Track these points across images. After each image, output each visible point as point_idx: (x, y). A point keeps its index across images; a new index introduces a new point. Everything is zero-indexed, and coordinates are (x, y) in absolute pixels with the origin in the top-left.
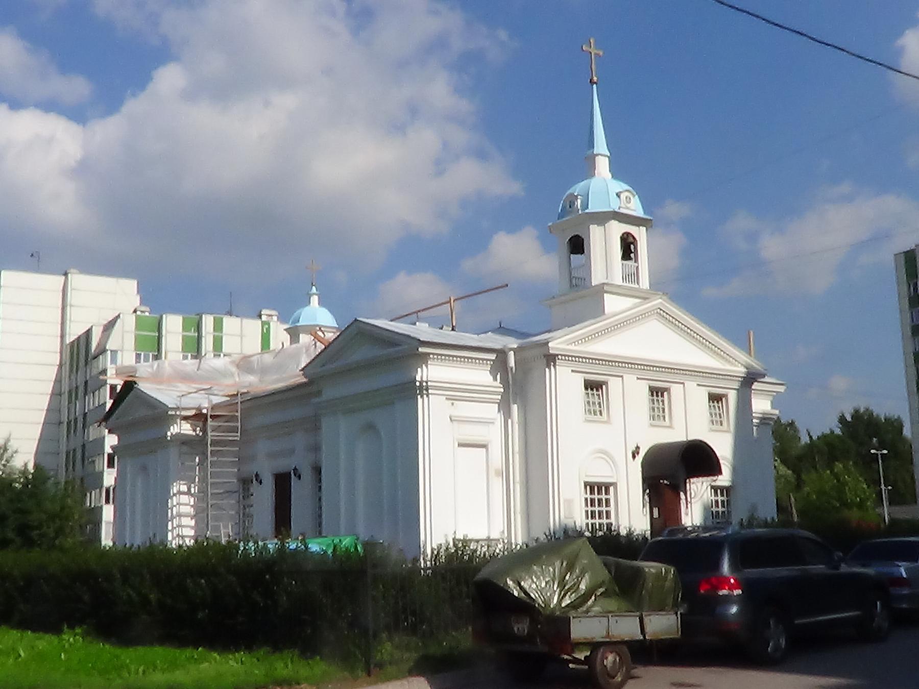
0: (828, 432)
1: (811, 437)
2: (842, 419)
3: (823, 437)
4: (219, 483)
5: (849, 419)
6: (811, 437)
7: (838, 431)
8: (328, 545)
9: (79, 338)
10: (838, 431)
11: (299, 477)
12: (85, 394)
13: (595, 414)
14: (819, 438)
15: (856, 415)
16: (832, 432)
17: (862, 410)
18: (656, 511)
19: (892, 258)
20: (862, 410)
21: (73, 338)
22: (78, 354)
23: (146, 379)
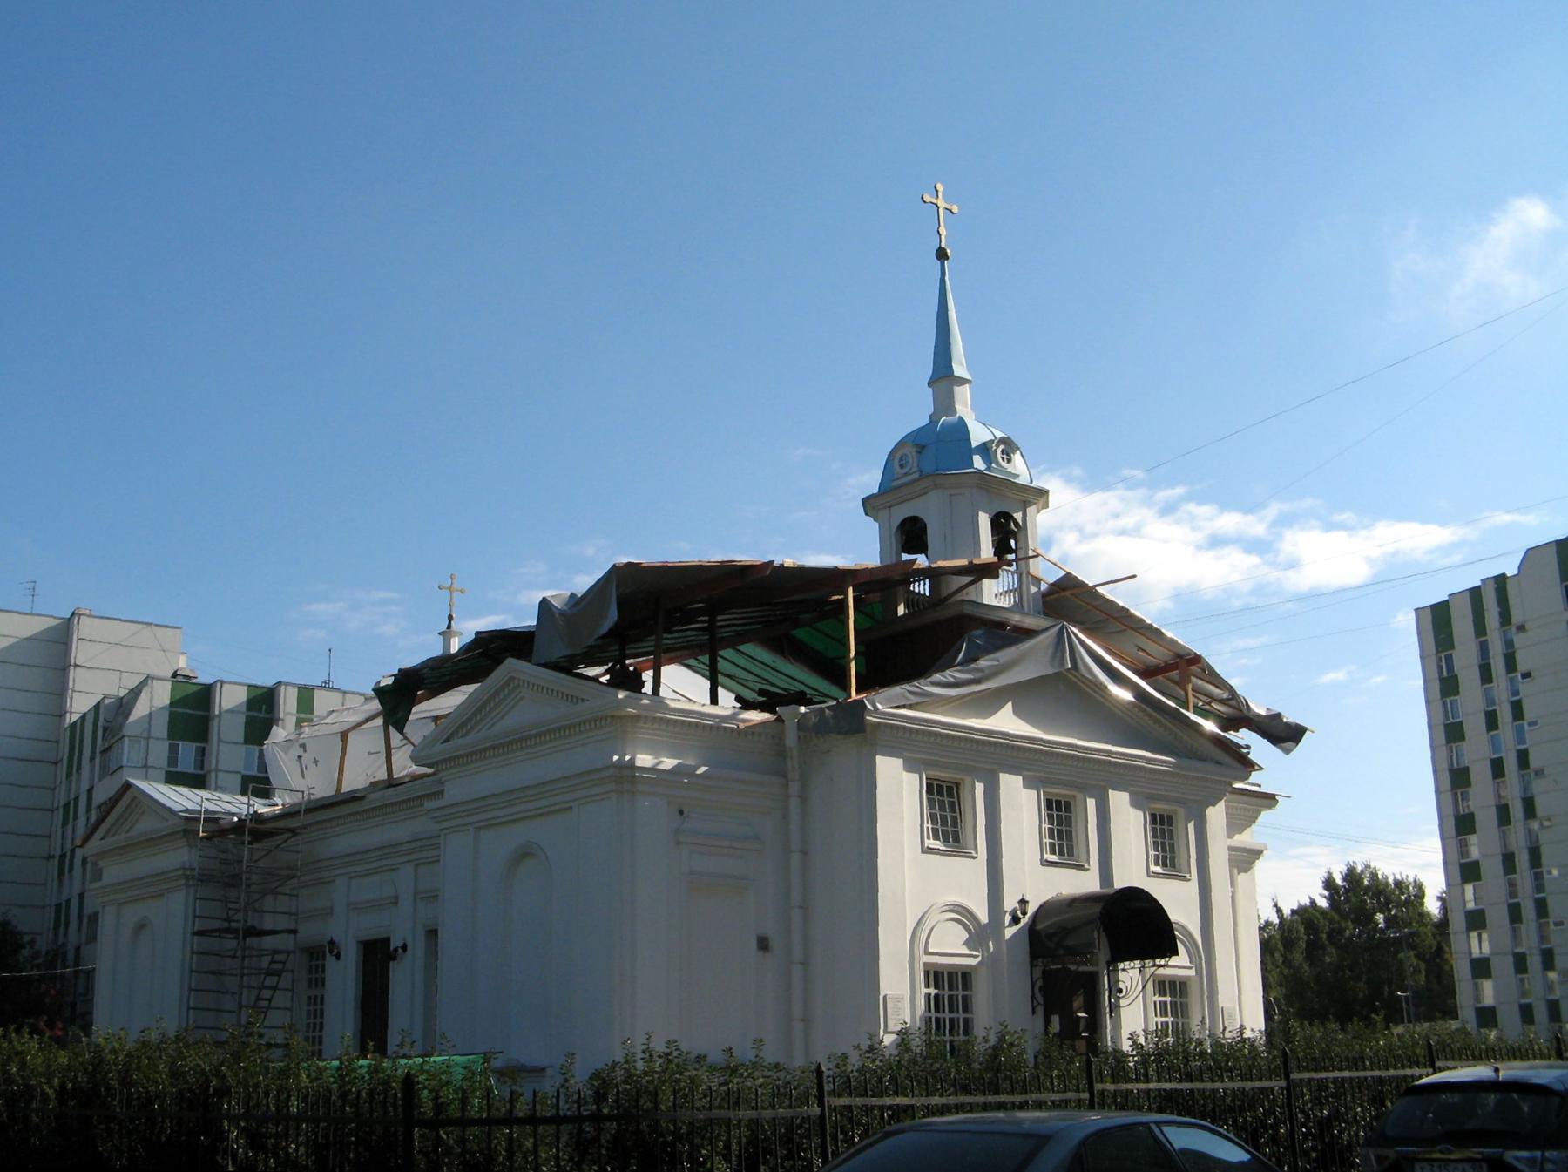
0: (1306, 902)
1: (1279, 911)
2: (1329, 883)
3: (1300, 912)
4: (950, 698)
5: (1339, 881)
6: (1279, 911)
7: (1323, 903)
8: (1245, 859)
9: (83, 717)
10: (1323, 903)
11: (338, 957)
12: (67, 806)
13: (1058, 802)
14: (1293, 912)
15: (1351, 875)
16: (1313, 902)
17: (1359, 869)
18: (1056, 1019)
19: (1412, 616)
20: (1359, 869)
21: (75, 717)
22: (82, 741)
23: (447, 644)
